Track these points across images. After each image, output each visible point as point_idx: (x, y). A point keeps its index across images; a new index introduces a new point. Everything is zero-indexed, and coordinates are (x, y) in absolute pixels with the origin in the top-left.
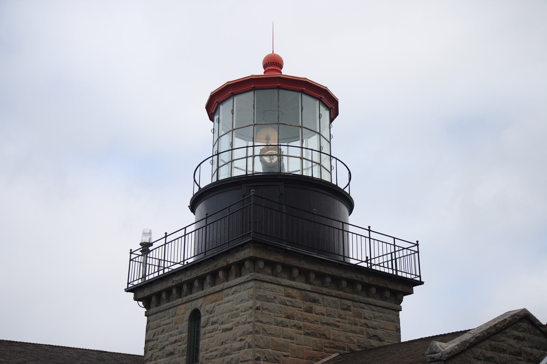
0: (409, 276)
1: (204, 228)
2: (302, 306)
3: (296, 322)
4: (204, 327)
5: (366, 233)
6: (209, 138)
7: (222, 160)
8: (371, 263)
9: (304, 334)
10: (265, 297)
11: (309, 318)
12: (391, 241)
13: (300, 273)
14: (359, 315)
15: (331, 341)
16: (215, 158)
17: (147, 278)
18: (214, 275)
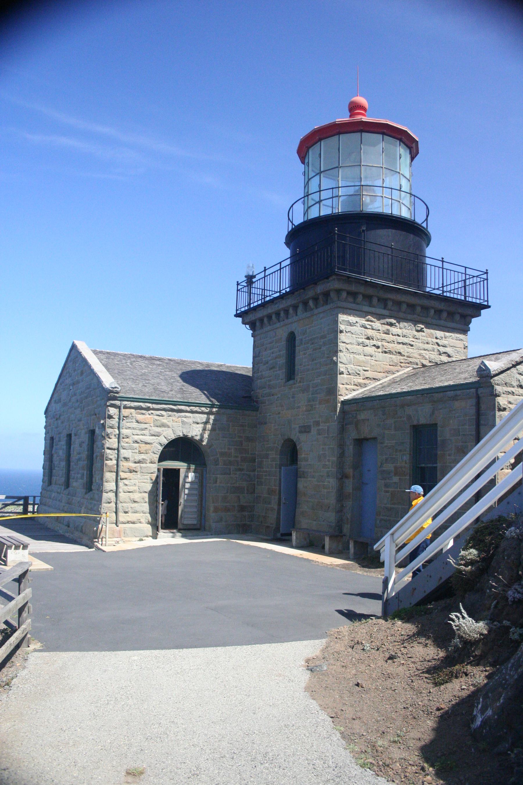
0: (478, 301)
1: (279, 271)
2: (380, 328)
3: (375, 342)
4: (298, 346)
5: (440, 264)
6: (301, 180)
7: (312, 199)
8: (443, 291)
9: (382, 352)
10: (348, 321)
11: (386, 339)
12: (462, 270)
13: (435, 312)
14: (431, 336)
15: (405, 358)
16: (306, 198)
17: (252, 306)
18: (295, 307)
